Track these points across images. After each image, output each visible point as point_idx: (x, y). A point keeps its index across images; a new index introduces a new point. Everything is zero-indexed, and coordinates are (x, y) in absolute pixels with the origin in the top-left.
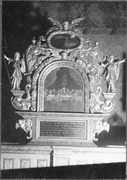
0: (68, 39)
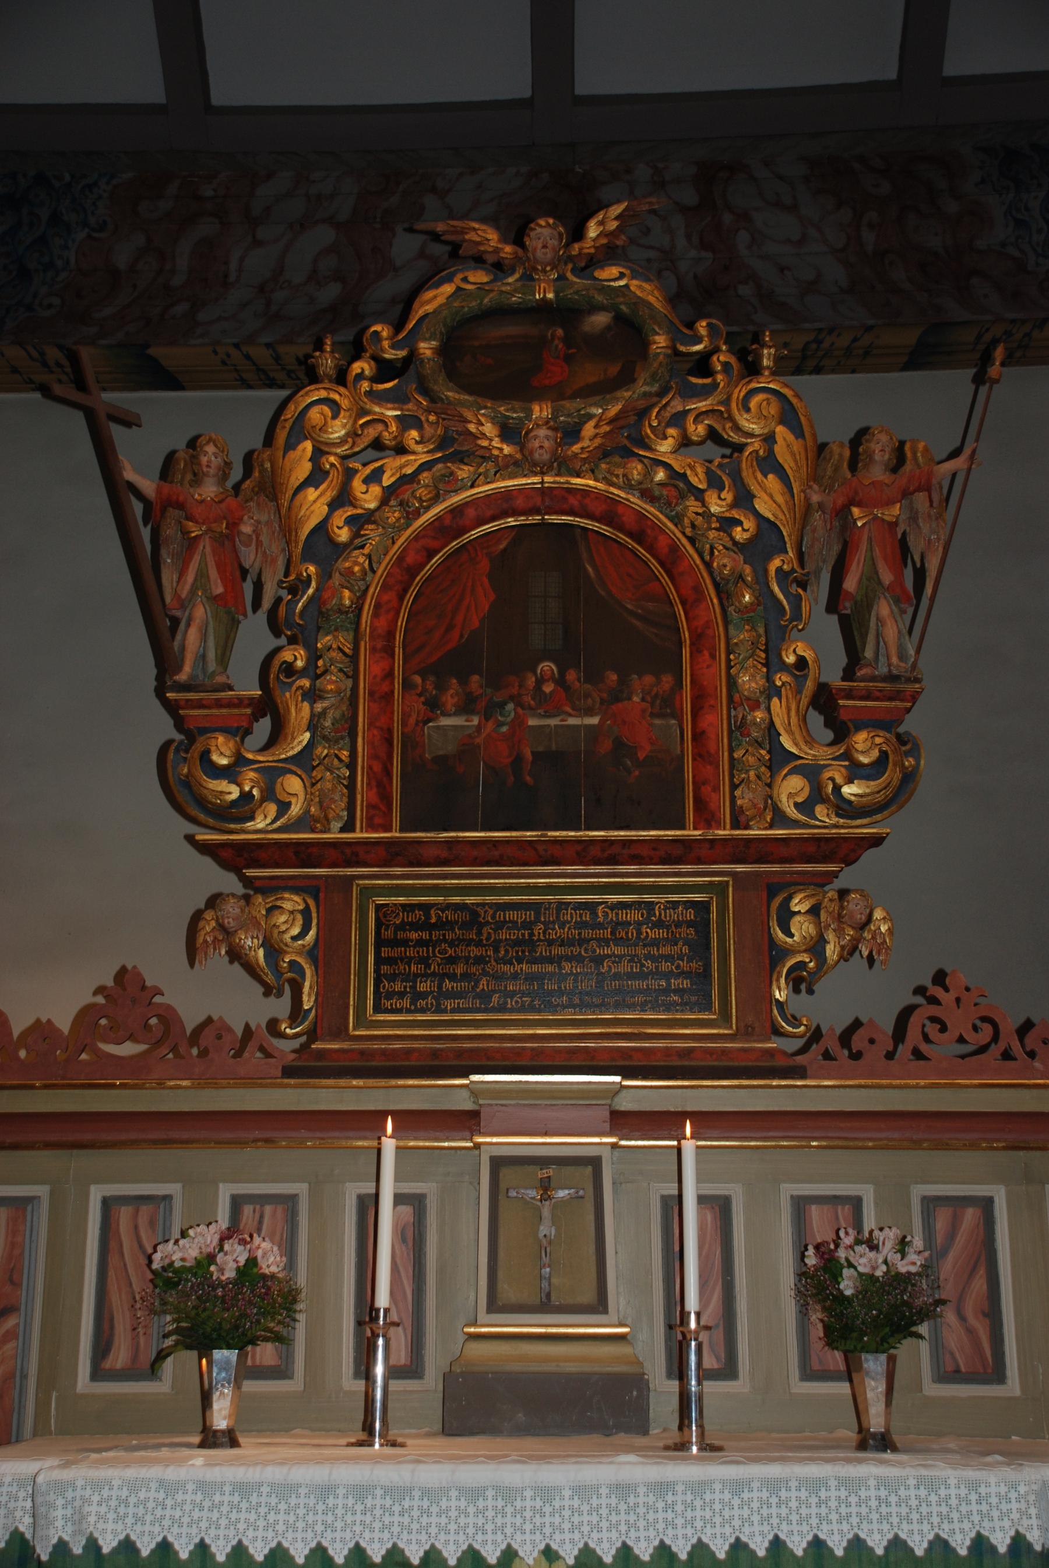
0: (567, 340)
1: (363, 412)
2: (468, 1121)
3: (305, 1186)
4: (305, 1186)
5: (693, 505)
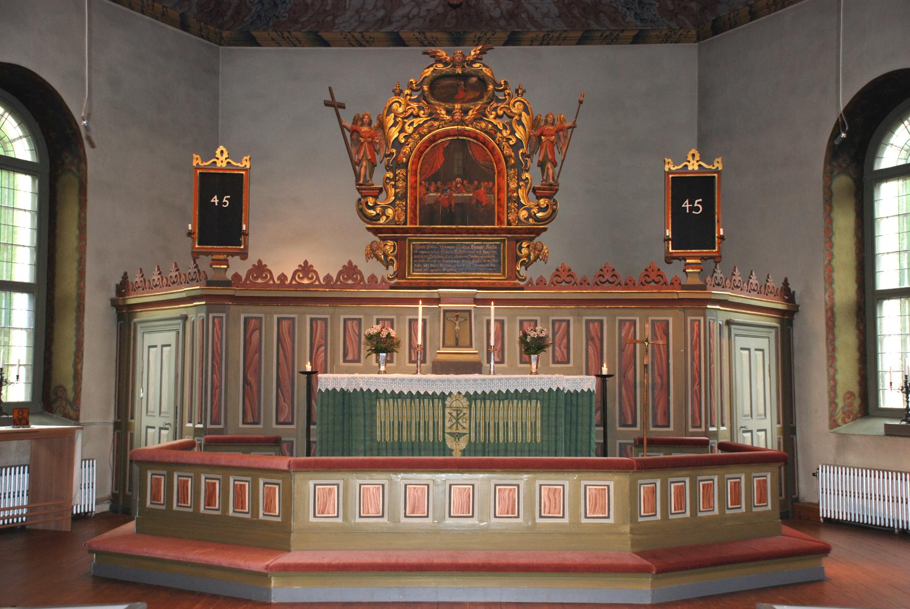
0: (465, 85)
1: (408, 105)
2: (438, 301)
5: (499, 135)
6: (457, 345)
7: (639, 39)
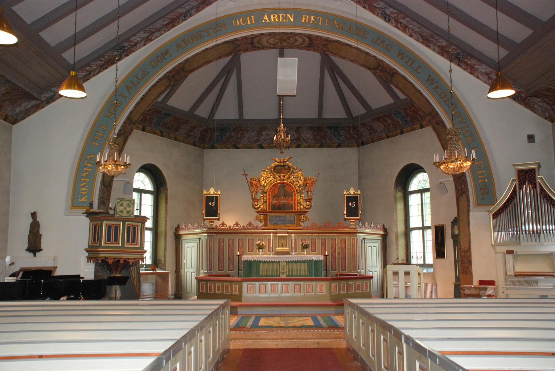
2: (276, 233)
3: (125, 246)
4: (125, 246)
6: (282, 246)
7: (339, 146)
